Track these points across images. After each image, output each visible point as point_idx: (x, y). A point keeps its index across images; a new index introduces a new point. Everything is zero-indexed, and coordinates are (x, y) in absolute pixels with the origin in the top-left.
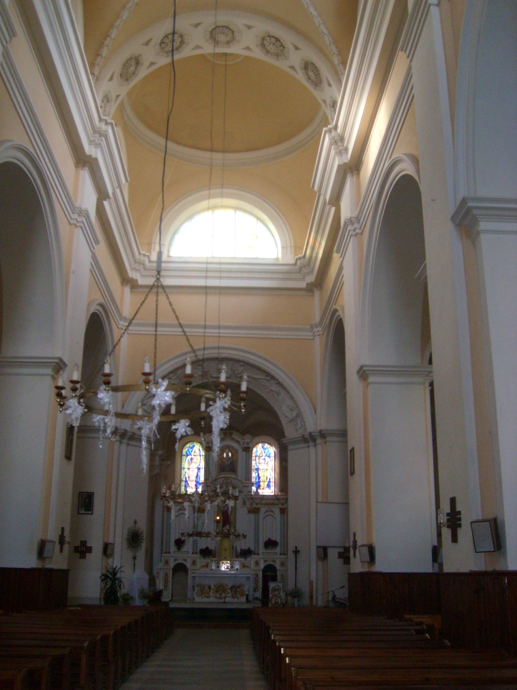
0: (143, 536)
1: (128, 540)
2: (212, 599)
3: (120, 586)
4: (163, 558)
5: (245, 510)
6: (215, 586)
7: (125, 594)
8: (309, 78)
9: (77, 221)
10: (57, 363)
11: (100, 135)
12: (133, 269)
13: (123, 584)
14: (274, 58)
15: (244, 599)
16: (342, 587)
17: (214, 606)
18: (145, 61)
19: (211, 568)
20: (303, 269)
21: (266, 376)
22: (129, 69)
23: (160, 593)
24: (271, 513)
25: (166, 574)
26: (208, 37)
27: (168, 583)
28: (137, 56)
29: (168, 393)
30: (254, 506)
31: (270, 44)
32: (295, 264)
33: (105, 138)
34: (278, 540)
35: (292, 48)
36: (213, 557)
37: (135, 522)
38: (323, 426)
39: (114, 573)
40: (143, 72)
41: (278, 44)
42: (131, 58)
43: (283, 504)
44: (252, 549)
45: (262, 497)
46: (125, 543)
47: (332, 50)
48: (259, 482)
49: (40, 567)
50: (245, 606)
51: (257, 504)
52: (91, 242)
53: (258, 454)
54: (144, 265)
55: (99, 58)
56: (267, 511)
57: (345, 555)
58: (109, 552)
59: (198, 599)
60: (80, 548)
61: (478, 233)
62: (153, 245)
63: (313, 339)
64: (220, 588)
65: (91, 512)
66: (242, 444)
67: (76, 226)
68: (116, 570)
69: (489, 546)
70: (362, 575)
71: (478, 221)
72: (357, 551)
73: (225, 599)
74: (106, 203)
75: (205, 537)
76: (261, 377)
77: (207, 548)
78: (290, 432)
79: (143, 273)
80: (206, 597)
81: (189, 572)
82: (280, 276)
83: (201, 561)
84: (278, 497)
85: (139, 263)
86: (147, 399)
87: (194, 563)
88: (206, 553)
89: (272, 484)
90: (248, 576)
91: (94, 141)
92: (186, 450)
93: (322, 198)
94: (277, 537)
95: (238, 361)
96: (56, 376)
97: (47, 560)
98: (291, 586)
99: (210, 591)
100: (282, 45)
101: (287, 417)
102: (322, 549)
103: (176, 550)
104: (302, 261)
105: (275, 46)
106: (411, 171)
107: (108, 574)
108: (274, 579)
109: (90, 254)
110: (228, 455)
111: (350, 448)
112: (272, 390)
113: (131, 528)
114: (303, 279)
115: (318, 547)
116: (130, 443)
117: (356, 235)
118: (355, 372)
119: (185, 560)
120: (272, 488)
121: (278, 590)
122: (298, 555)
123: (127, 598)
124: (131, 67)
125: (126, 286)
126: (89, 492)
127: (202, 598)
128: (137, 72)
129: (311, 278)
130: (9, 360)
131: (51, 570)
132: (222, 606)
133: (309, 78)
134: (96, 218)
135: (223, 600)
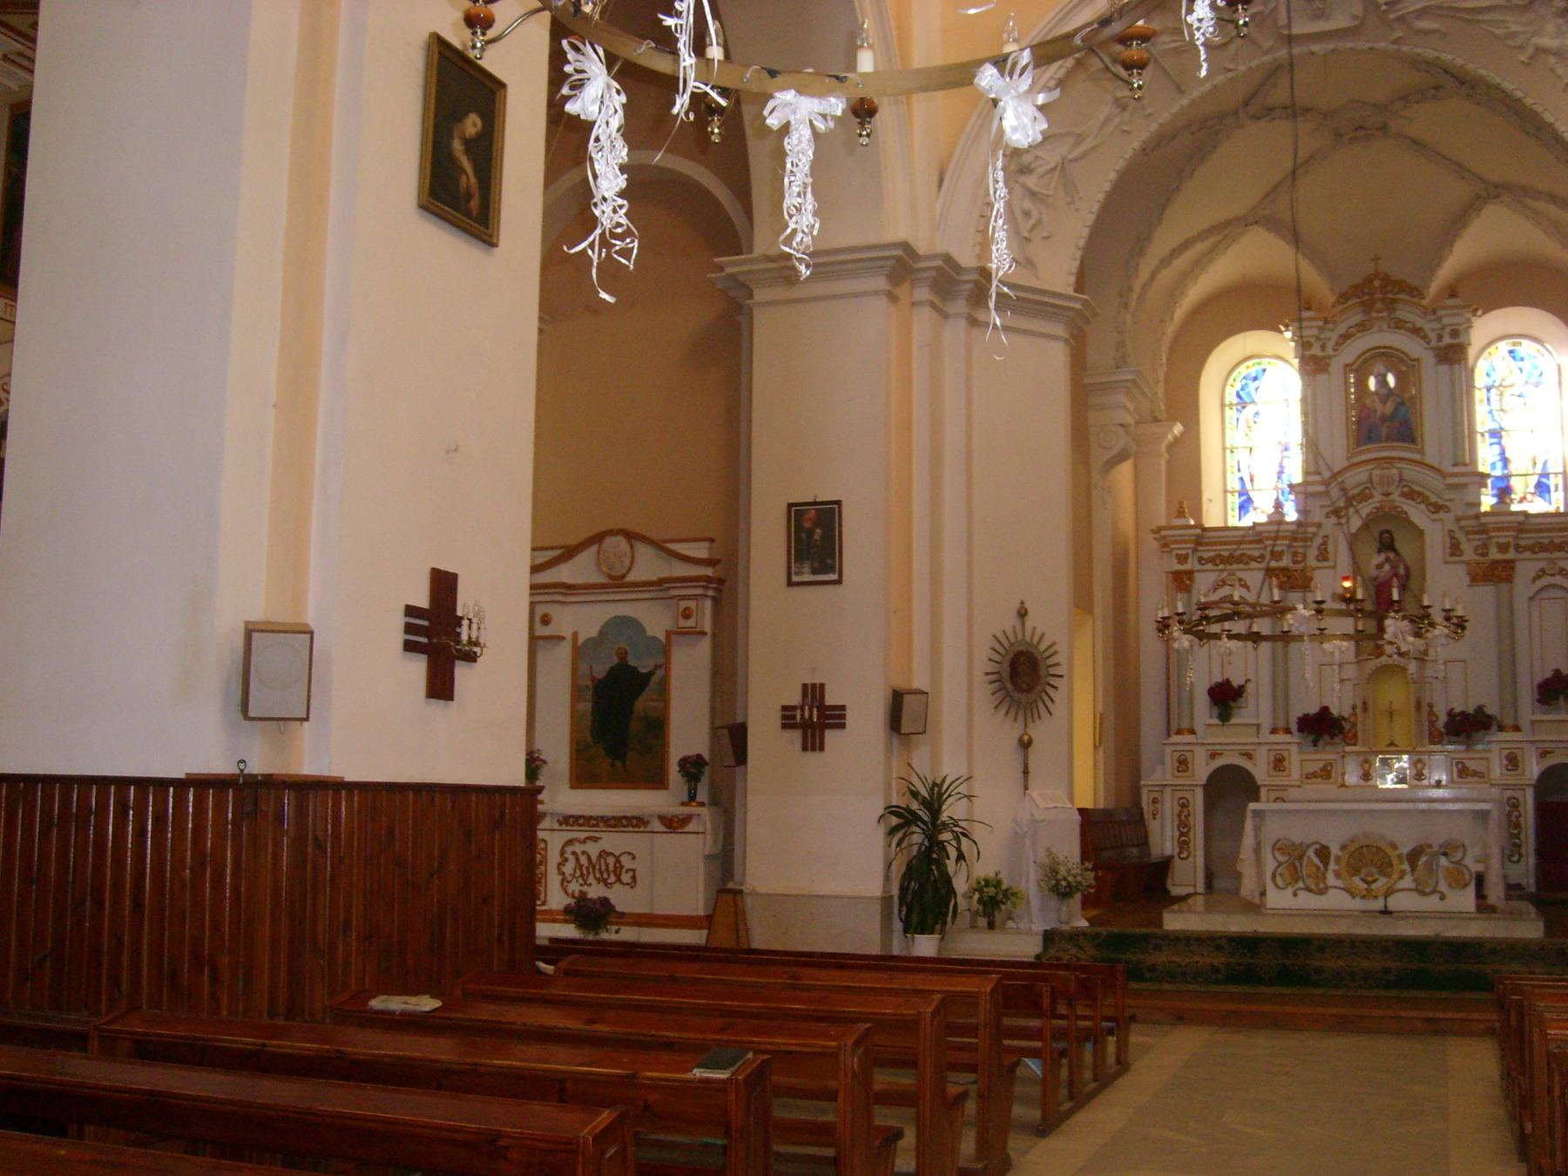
1: (996, 678)
2: (1336, 899)
5: (1459, 574)
6: (1343, 848)
10: (898, 259)
15: (1466, 900)
19: (1343, 779)
23: (1164, 866)
30: (1494, 554)
37: (1022, 614)
39: (933, 803)
44: (1492, 709)
45: (1522, 518)
46: (984, 695)
48: (1506, 477)
50: (1476, 930)
51: (1503, 548)
53: (1496, 378)
59: (1277, 898)
60: (798, 713)
65: (834, 577)
66: (1432, 336)
73: (1386, 898)
77: (1325, 710)
80: (1309, 890)
83: (1300, 756)
87: (1279, 763)
92: (1238, 386)
99: (1326, 869)
103: (1216, 721)
107: (915, 806)
110: (1382, 382)
112: (1541, 51)
119: (1248, 756)
127: (1295, 895)
135: (1378, 904)
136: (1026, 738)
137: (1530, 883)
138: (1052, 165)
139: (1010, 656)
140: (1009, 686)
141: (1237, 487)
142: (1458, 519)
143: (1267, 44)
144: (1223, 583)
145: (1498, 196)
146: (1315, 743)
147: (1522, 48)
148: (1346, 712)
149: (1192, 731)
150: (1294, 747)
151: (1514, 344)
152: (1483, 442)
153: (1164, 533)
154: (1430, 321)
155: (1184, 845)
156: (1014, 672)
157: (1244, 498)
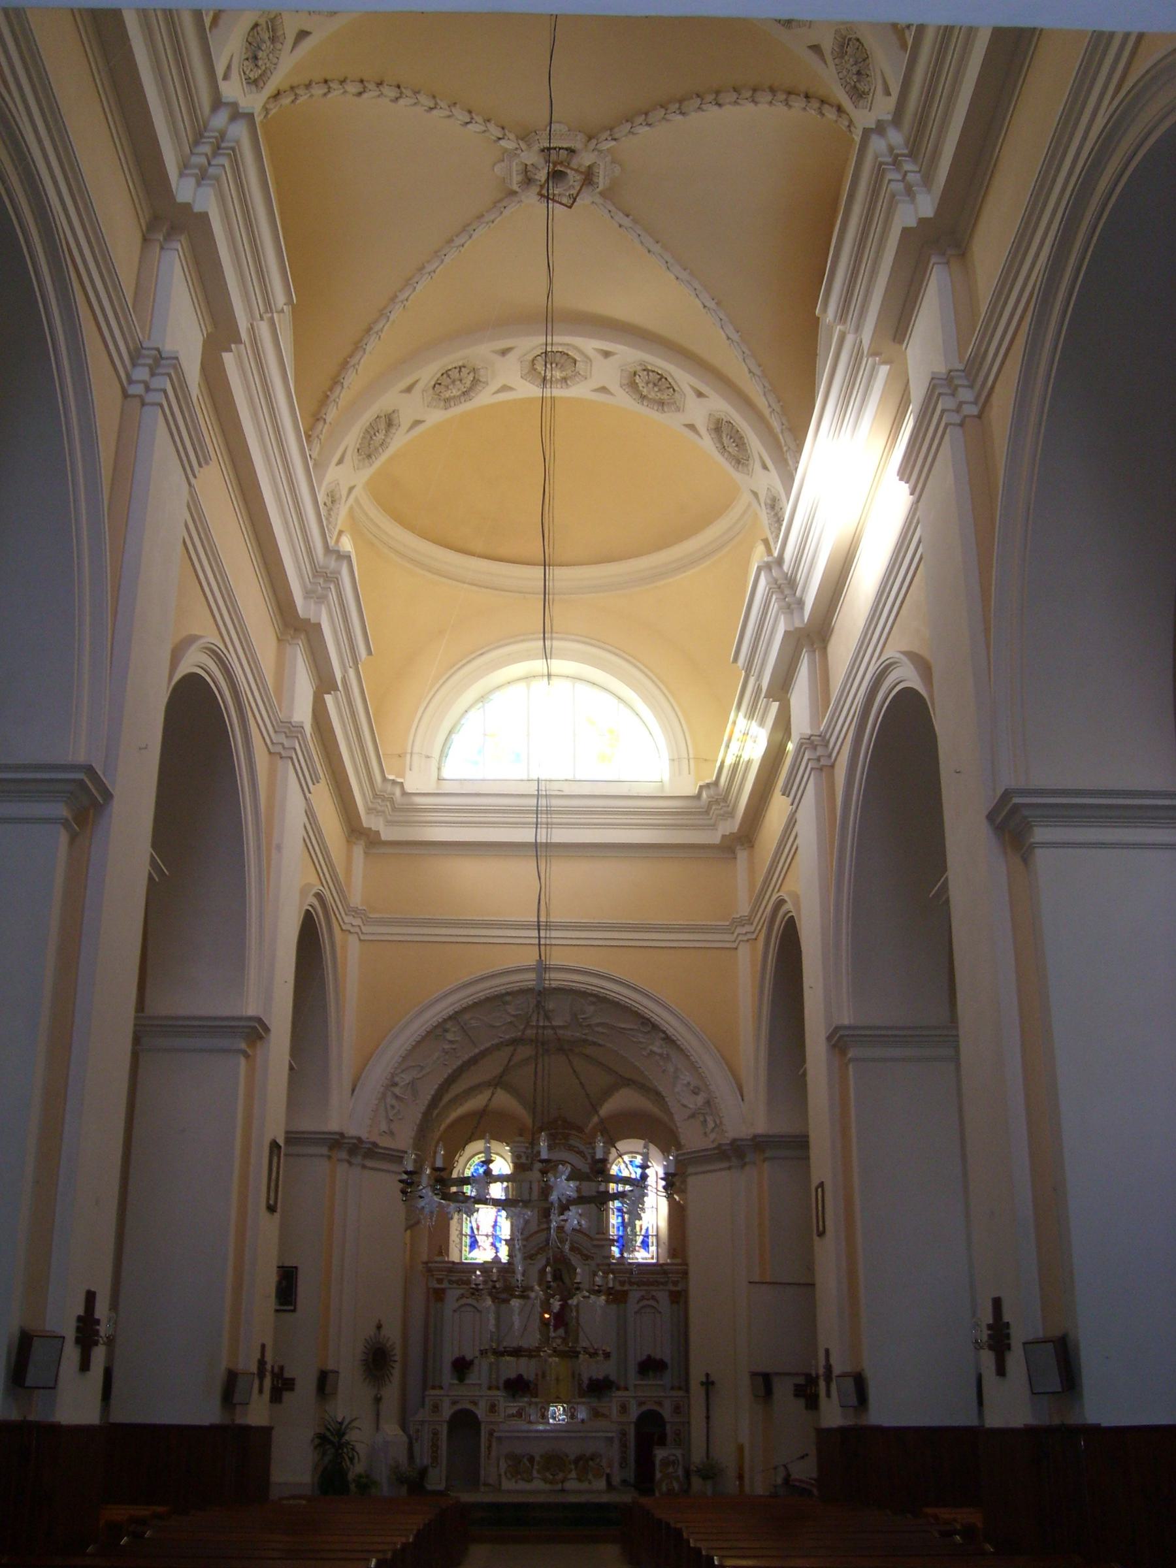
0: (395, 1355)
3: (351, 1460)
4: (427, 1399)
6: (541, 1456)
7: (360, 1476)
9: (284, 748)
11: (327, 579)
13: (357, 1453)
14: (656, 408)
15: (601, 1484)
16: (803, 1457)
17: (541, 1499)
18: (405, 419)
20: (714, 807)
21: (643, 1023)
22: (374, 438)
24: (652, 1302)
25: (436, 1434)
27: (439, 1452)
28: (389, 412)
29: (572, 1184)
31: (647, 383)
32: (698, 797)
33: (335, 586)
34: (667, 1359)
36: (532, 1397)
37: (379, 1327)
38: (761, 1126)
39: (341, 1434)
40: (399, 440)
43: (675, 1283)
44: (613, 1378)
49: (218, 1422)
50: (605, 1499)
54: (392, 801)
55: (320, 425)
56: (642, 1298)
57: (808, 1391)
59: (507, 1485)
61: (1032, 847)
63: (736, 949)
64: (554, 1463)
66: (589, 1157)
68: (343, 1427)
69: (1053, 1382)
70: (844, 1432)
72: (834, 1386)
74: (329, 698)
75: (525, 1356)
78: (694, 1138)
79: (389, 818)
80: (523, 1479)
81: (483, 1427)
82: (668, 820)
84: (665, 1267)
85: (384, 799)
86: (402, 1072)
87: (493, 1408)
88: (517, 1387)
90: (610, 1435)
94: (663, 1352)
95: (584, 994)
98: (698, 1456)
101: (685, 1106)
103: (456, 1382)
104: (712, 791)
105: (656, 389)
107: (328, 1434)
114: (713, 827)
115: (754, 1375)
116: (369, 1163)
117: (821, 769)
120: (653, 1249)
121: (673, 1463)
123: (365, 1485)
124: (377, 434)
126: (287, 1267)
128: (388, 440)
129: (732, 826)
132: (559, 1499)
134: (312, 727)
135: (559, 1487)
136: (379, 1396)
137: (632, 1480)
138: (407, 1082)
141: (469, 1232)
142: (598, 1265)
144: (462, 1296)
145: (629, 1085)
146: (514, 1396)
147: (644, 1049)
148: (532, 1378)
149: (441, 1388)
150: (499, 1395)
151: (633, 1157)
152: (614, 1214)
153: (430, 1265)
154: (588, 1148)
155: (435, 1459)
157: (473, 1239)
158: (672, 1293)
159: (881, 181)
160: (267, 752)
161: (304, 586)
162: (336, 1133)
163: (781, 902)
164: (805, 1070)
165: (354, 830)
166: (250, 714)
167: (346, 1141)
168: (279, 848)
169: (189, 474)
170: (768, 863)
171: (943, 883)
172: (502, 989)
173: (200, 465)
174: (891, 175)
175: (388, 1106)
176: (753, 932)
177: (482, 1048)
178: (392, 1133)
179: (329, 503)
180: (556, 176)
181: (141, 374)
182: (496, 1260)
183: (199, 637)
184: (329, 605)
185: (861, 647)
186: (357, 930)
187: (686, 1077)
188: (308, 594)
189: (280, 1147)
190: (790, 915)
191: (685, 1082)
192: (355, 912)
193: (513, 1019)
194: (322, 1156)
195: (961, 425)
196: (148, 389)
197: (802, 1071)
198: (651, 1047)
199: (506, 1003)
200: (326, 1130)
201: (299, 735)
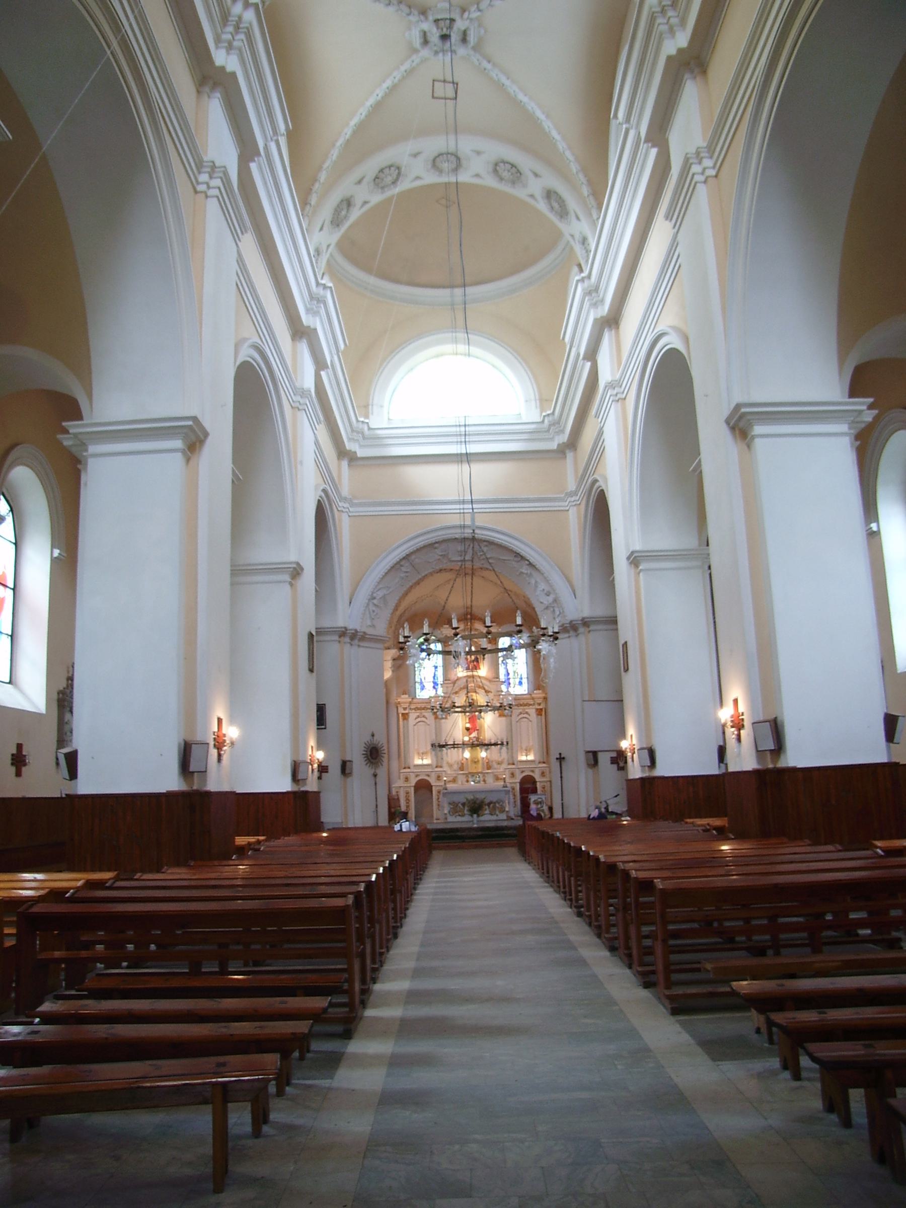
0: (383, 750)
4: (402, 774)
8: (552, 208)
9: (300, 404)
10: (294, 568)
11: (318, 301)
12: (350, 439)
16: (616, 796)
18: (358, 202)
24: (423, 719)
26: (430, 166)
32: (543, 422)
35: (531, 175)
37: (373, 735)
38: (586, 613)
40: (355, 214)
41: (514, 170)
42: (342, 201)
47: (580, 180)
50: (505, 824)
52: (314, 423)
54: (363, 433)
58: (347, 771)
61: (753, 437)
62: (370, 407)
63: (568, 510)
65: (323, 727)
67: (299, 410)
71: (753, 426)
74: (323, 373)
76: (509, 558)
79: (361, 444)
80: (459, 815)
81: (434, 788)
85: (358, 432)
89: (525, 681)
91: (312, 309)
93: (574, 350)
96: (293, 582)
97: (301, 782)
100: (518, 171)
101: (541, 603)
102: (591, 754)
104: (551, 418)
106: (678, 345)
108: (534, 791)
109: (313, 439)
111: (622, 642)
112: (522, 573)
113: (368, 742)
116: (361, 644)
118: (625, 559)
121: (540, 803)
122: (563, 763)
125: (343, 460)
129: (564, 438)
130: (241, 568)
131: (307, 792)
133: (552, 208)
139: (369, 750)
140: (370, 757)
143: (445, 562)
149: (409, 768)
156: (371, 754)
158: (537, 709)
159: (654, 24)
160: (290, 407)
161: (305, 306)
162: (341, 627)
163: (596, 481)
164: (614, 578)
165: (342, 453)
166: (280, 386)
167: (348, 632)
168: (301, 463)
169: (236, 239)
170: (587, 457)
171: (697, 463)
172: (433, 540)
173: (242, 233)
174: (659, 21)
175: (371, 611)
176: (578, 500)
177: (423, 575)
178: (373, 626)
179: (316, 256)
180: (445, 37)
181: (204, 177)
182: (437, 696)
183: (247, 339)
184: (321, 316)
185: (642, 325)
186: (347, 510)
187: (542, 586)
188: (308, 311)
189: (313, 635)
190: (601, 488)
191: (541, 589)
192: (344, 500)
193: (439, 557)
194: (334, 641)
195: (705, 182)
196: (209, 187)
197: (612, 578)
198: (521, 570)
199: (435, 548)
200: (335, 626)
201: (309, 396)
